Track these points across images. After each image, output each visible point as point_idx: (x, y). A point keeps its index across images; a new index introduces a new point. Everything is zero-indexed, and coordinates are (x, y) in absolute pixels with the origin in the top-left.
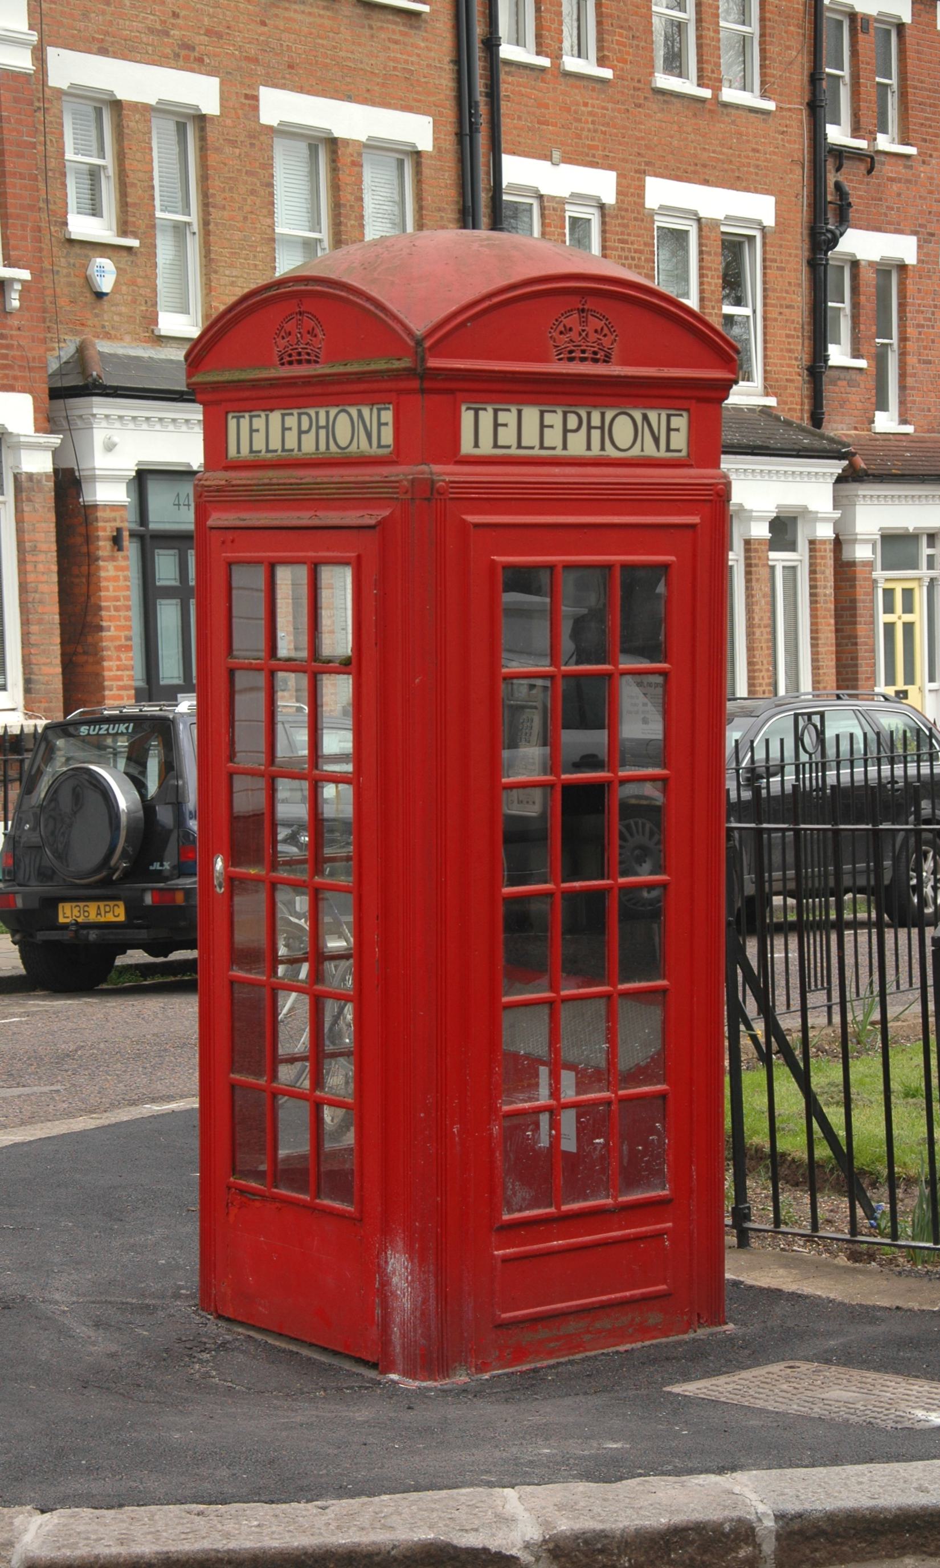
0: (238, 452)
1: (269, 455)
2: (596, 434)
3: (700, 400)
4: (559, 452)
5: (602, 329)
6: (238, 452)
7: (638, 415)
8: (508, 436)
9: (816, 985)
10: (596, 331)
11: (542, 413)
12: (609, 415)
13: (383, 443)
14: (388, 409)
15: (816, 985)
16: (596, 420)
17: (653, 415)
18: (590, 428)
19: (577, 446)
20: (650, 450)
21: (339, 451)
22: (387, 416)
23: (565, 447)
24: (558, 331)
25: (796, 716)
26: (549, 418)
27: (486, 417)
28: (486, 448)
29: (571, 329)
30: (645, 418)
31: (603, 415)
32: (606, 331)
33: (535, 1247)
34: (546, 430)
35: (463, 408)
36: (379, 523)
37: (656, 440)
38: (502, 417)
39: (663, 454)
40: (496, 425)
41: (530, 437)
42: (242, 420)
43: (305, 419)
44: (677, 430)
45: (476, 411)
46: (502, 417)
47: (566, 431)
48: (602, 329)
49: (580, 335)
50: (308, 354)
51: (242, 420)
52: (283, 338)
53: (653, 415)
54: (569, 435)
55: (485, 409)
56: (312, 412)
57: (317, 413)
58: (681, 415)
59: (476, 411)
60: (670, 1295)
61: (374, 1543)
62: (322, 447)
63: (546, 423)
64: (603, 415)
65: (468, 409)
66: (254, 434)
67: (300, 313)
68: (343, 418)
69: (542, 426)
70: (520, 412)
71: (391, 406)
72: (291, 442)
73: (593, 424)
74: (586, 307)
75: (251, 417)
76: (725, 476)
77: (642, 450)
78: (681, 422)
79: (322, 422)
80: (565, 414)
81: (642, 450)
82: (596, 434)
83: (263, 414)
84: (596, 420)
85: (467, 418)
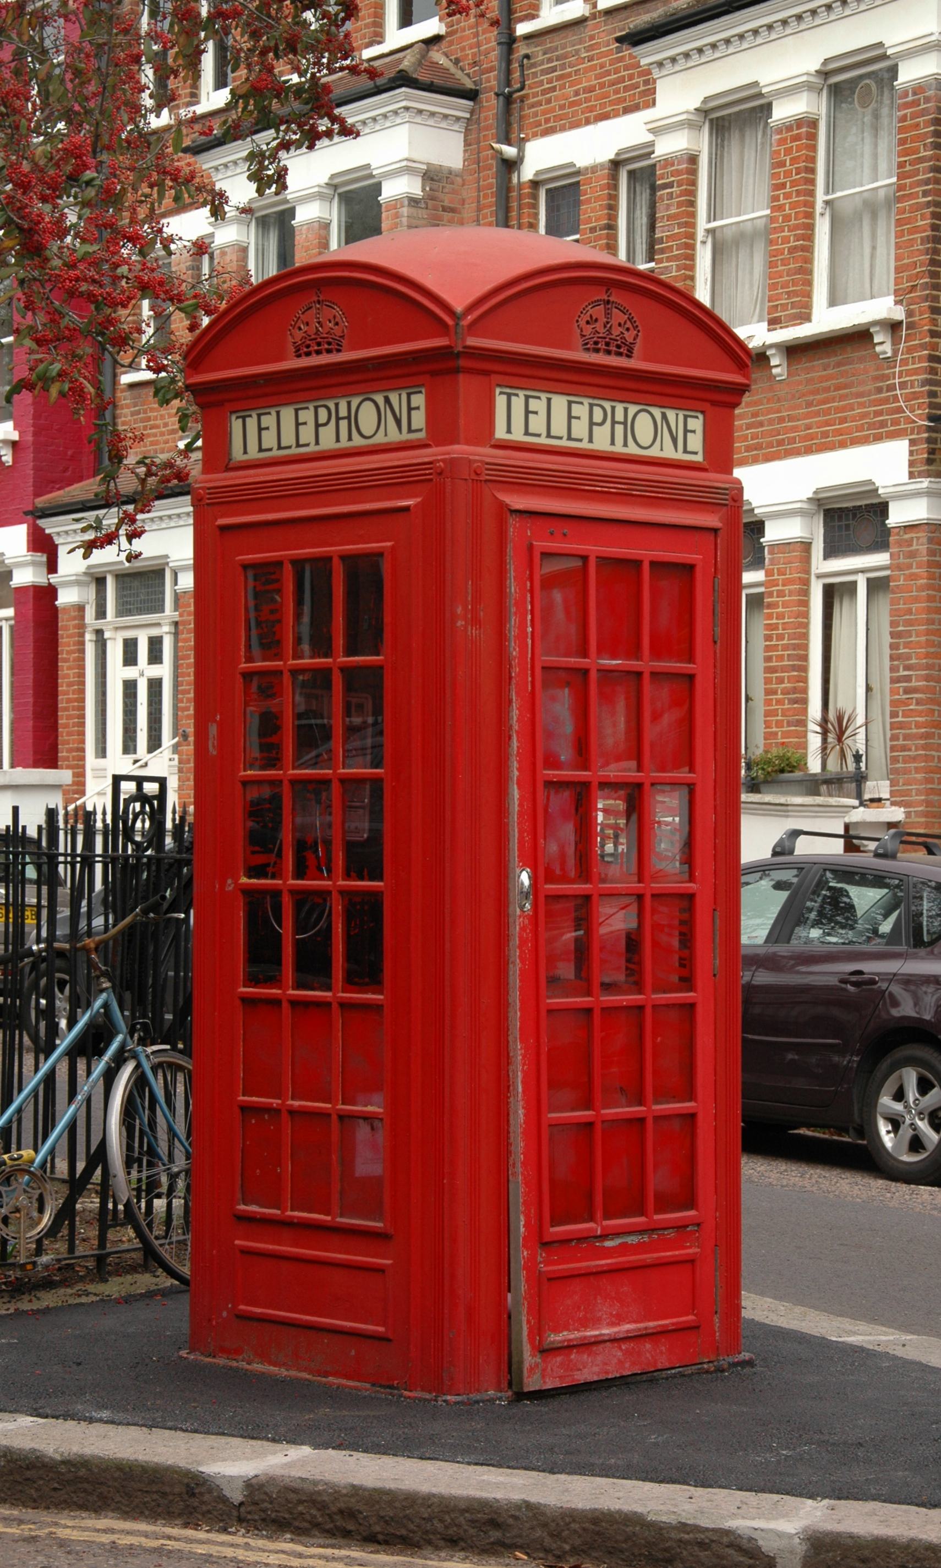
2: (619, 429)
3: (714, 403)
4: (585, 445)
5: (625, 323)
7: (380, 399)
8: (537, 424)
10: (588, 323)
11: (570, 403)
13: (414, 427)
14: (420, 392)
16: (619, 416)
18: (614, 422)
20: (669, 453)
22: (419, 400)
23: (591, 441)
26: (576, 410)
27: (518, 403)
32: (628, 325)
33: (271, 1247)
34: (573, 421)
35: (498, 390)
38: (533, 405)
40: (527, 412)
41: (559, 427)
42: (248, 420)
43: (323, 414)
44: (694, 432)
45: (509, 396)
46: (533, 405)
47: (592, 424)
49: (605, 327)
50: (329, 343)
51: (248, 420)
53: (394, 397)
54: (595, 428)
56: (331, 405)
57: (337, 405)
58: (697, 417)
59: (509, 396)
60: (698, 1327)
61: (34, 1451)
66: (264, 432)
67: (319, 302)
68: (368, 406)
69: (570, 417)
70: (549, 400)
71: (423, 390)
74: (611, 299)
75: (259, 416)
76: (738, 482)
78: (696, 423)
79: (343, 412)
80: (591, 406)
81: (386, 435)
82: (619, 429)
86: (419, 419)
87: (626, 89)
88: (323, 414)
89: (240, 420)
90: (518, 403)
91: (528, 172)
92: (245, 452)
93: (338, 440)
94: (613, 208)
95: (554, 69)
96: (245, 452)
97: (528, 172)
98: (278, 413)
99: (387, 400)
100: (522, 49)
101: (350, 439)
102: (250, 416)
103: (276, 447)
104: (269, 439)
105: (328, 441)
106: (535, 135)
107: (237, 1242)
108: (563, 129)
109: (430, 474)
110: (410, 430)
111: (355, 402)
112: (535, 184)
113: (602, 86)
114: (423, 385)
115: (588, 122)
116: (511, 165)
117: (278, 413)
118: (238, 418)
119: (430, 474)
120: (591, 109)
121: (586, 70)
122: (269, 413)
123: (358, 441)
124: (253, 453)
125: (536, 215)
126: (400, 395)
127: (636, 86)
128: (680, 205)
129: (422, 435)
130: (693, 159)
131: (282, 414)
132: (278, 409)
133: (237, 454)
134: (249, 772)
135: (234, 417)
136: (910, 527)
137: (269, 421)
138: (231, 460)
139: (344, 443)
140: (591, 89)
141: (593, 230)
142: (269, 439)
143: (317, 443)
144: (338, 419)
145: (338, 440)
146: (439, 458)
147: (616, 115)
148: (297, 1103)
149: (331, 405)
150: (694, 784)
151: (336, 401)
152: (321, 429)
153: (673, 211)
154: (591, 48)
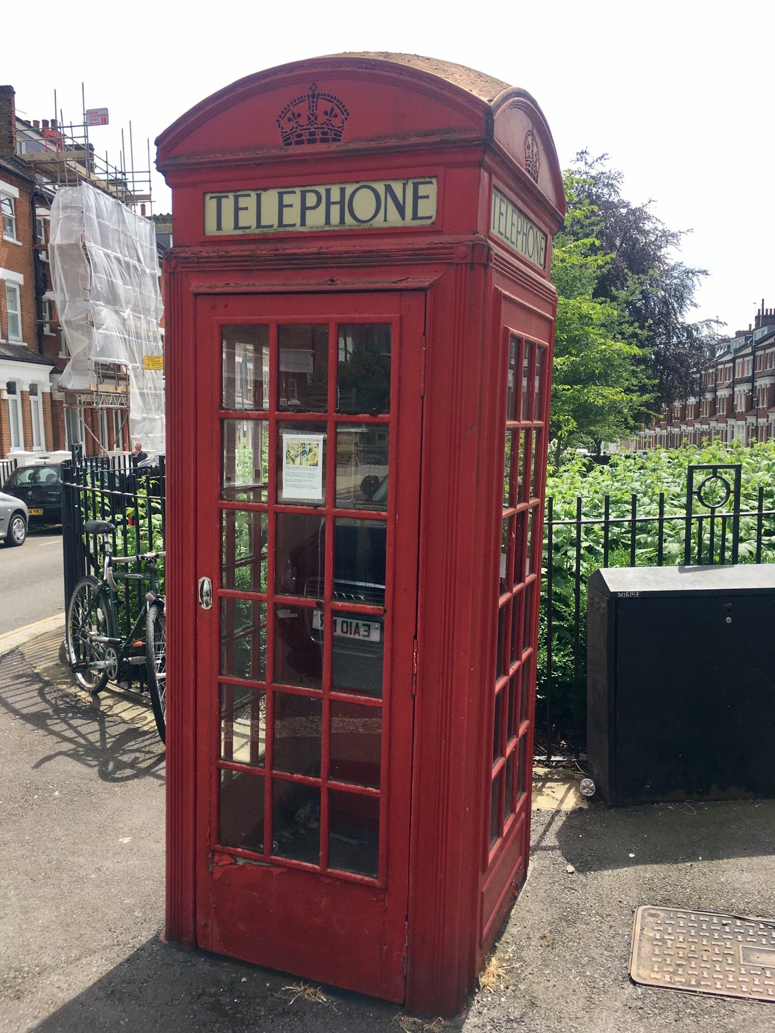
0: (219, 227)
1: (282, 229)
5: (332, 109)
6: (219, 227)
7: (380, 187)
9: (116, 413)
10: (326, 113)
12: (350, 189)
15: (116, 413)
16: (335, 196)
17: (397, 187)
19: (316, 219)
21: (355, 222)
24: (286, 118)
25: (691, 469)
28: (228, 228)
29: (299, 115)
30: (389, 189)
31: (343, 191)
34: (240, 212)
36: (431, 286)
37: (401, 209)
38: (243, 202)
39: (409, 221)
42: (223, 200)
43: (311, 199)
46: (243, 202)
48: (332, 109)
52: (290, 120)
53: (397, 187)
54: (308, 212)
55: (227, 197)
56: (322, 190)
62: (335, 218)
63: (241, 205)
64: (343, 191)
65: (211, 198)
72: (292, 216)
73: (332, 200)
77: (385, 220)
81: (385, 220)
83: (253, 194)
84: (335, 196)
85: (211, 205)
86: (428, 208)
90: (228, 204)
98: (259, 197)
114: (436, 177)
126: (404, 185)
135: (208, 197)
145: (403, 219)
150: (275, 604)
151: (328, 187)
152: (240, 212)
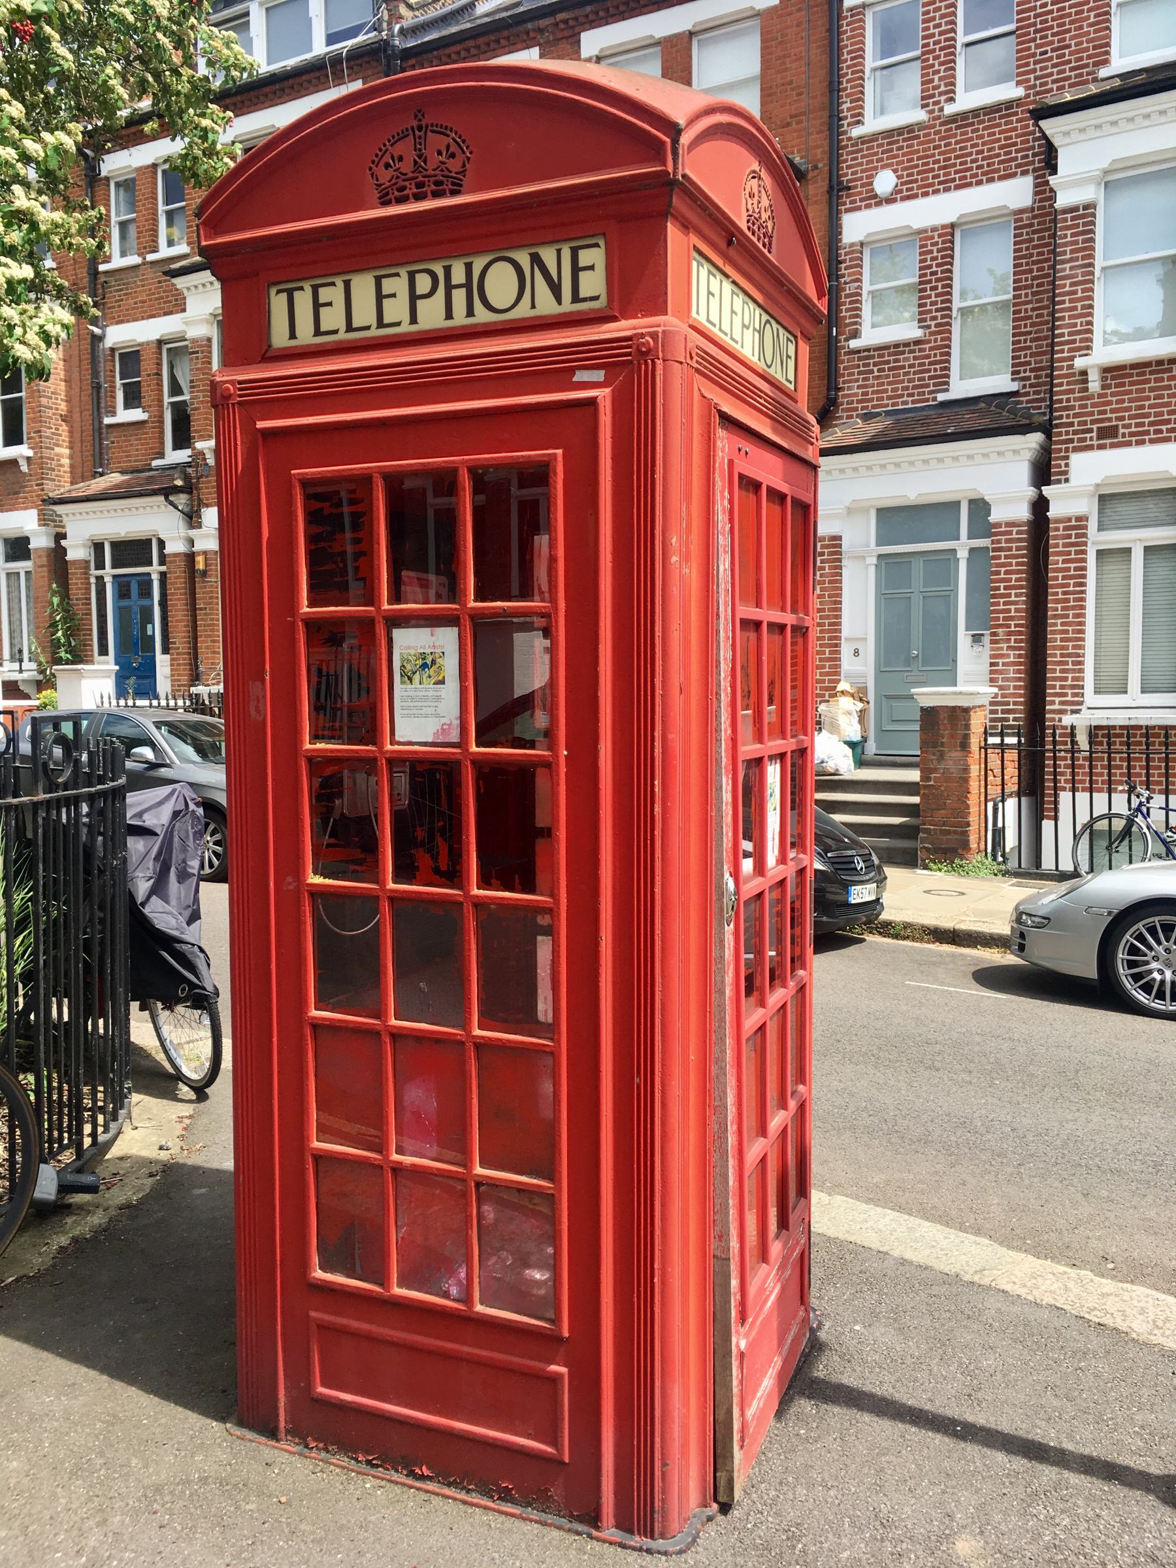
14: (597, 245)
22: (594, 256)
42: (296, 294)
43: (423, 283)
51: (296, 294)
53: (548, 255)
71: (602, 243)
81: (533, 306)
86: (594, 284)
87: (165, 303)
88: (423, 283)
89: (284, 296)
91: (109, 342)
92: (293, 336)
93: (449, 315)
94: (159, 364)
95: (121, 290)
96: (293, 336)
97: (109, 342)
98: (347, 284)
99: (536, 259)
100: (102, 279)
101: (470, 312)
102: (302, 289)
103: (343, 328)
104: (333, 318)
105: (431, 315)
106: (112, 324)
107: (313, 1314)
108: (128, 321)
109: (629, 354)
110: (576, 298)
111: (479, 264)
112: (112, 350)
113: (151, 300)
115: (143, 319)
116: (101, 338)
117: (347, 284)
118: (279, 292)
119: (629, 354)
120: (145, 312)
121: (141, 292)
122: (333, 284)
123: (482, 316)
124: (305, 335)
125: (114, 366)
126: (559, 251)
127: (170, 302)
128: (203, 363)
129: (601, 303)
130: (209, 340)
131: (352, 284)
132: (347, 277)
133: (279, 338)
134: (320, 746)
135: (273, 291)
136: (176, 555)
137: (333, 294)
138: (270, 346)
139: (460, 318)
140: (144, 302)
141: (149, 375)
142: (333, 318)
143: (414, 320)
144: (449, 288)
145: (449, 315)
146: (644, 331)
147: (160, 316)
148: (408, 1160)
149: (438, 269)
152: (419, 303)
153: (199, 366)
154: (142, 280)
